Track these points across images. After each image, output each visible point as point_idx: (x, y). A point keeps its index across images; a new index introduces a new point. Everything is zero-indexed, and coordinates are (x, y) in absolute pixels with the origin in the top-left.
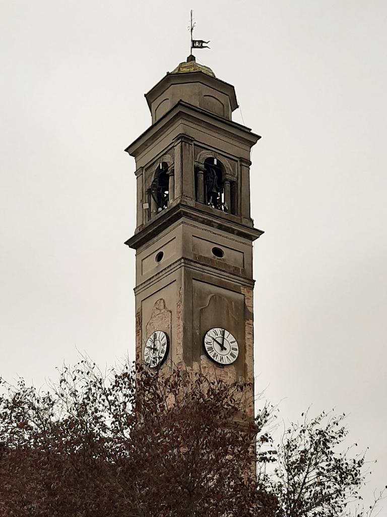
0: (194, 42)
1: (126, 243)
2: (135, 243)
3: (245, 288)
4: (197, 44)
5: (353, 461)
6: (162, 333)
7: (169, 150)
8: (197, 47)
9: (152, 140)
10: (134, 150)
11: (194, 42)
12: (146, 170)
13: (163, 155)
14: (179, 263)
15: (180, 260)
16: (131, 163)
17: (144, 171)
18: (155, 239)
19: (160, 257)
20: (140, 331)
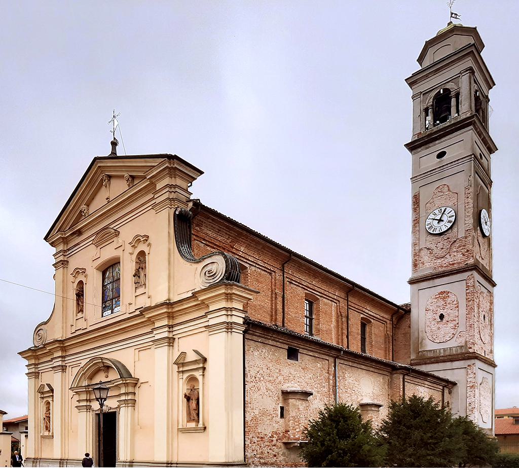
0: (452, 14)
1: (406, 145)
2: (412, 147)
3: (235, 240)
4: (453, 15)
5: (490, 351)
6: (453, 211)
7: (455, 79)
8: (453, 17)
9: (435, 72)
10: (412, 81)
11: (452, 14)
12: (423, 94)
13: (445, 83)
14: (469, 158)
15: (471, 155)
16: (410, 92)
17: (422, 95)
18: (437, 142)
19: (441, 155)
20: (418, 209)
